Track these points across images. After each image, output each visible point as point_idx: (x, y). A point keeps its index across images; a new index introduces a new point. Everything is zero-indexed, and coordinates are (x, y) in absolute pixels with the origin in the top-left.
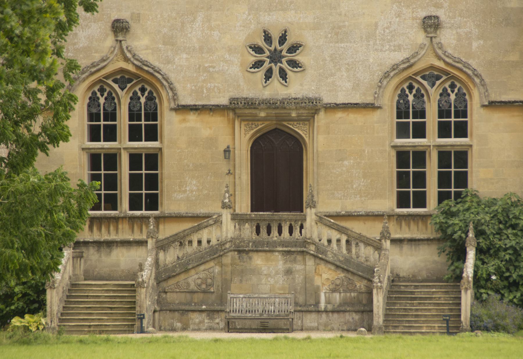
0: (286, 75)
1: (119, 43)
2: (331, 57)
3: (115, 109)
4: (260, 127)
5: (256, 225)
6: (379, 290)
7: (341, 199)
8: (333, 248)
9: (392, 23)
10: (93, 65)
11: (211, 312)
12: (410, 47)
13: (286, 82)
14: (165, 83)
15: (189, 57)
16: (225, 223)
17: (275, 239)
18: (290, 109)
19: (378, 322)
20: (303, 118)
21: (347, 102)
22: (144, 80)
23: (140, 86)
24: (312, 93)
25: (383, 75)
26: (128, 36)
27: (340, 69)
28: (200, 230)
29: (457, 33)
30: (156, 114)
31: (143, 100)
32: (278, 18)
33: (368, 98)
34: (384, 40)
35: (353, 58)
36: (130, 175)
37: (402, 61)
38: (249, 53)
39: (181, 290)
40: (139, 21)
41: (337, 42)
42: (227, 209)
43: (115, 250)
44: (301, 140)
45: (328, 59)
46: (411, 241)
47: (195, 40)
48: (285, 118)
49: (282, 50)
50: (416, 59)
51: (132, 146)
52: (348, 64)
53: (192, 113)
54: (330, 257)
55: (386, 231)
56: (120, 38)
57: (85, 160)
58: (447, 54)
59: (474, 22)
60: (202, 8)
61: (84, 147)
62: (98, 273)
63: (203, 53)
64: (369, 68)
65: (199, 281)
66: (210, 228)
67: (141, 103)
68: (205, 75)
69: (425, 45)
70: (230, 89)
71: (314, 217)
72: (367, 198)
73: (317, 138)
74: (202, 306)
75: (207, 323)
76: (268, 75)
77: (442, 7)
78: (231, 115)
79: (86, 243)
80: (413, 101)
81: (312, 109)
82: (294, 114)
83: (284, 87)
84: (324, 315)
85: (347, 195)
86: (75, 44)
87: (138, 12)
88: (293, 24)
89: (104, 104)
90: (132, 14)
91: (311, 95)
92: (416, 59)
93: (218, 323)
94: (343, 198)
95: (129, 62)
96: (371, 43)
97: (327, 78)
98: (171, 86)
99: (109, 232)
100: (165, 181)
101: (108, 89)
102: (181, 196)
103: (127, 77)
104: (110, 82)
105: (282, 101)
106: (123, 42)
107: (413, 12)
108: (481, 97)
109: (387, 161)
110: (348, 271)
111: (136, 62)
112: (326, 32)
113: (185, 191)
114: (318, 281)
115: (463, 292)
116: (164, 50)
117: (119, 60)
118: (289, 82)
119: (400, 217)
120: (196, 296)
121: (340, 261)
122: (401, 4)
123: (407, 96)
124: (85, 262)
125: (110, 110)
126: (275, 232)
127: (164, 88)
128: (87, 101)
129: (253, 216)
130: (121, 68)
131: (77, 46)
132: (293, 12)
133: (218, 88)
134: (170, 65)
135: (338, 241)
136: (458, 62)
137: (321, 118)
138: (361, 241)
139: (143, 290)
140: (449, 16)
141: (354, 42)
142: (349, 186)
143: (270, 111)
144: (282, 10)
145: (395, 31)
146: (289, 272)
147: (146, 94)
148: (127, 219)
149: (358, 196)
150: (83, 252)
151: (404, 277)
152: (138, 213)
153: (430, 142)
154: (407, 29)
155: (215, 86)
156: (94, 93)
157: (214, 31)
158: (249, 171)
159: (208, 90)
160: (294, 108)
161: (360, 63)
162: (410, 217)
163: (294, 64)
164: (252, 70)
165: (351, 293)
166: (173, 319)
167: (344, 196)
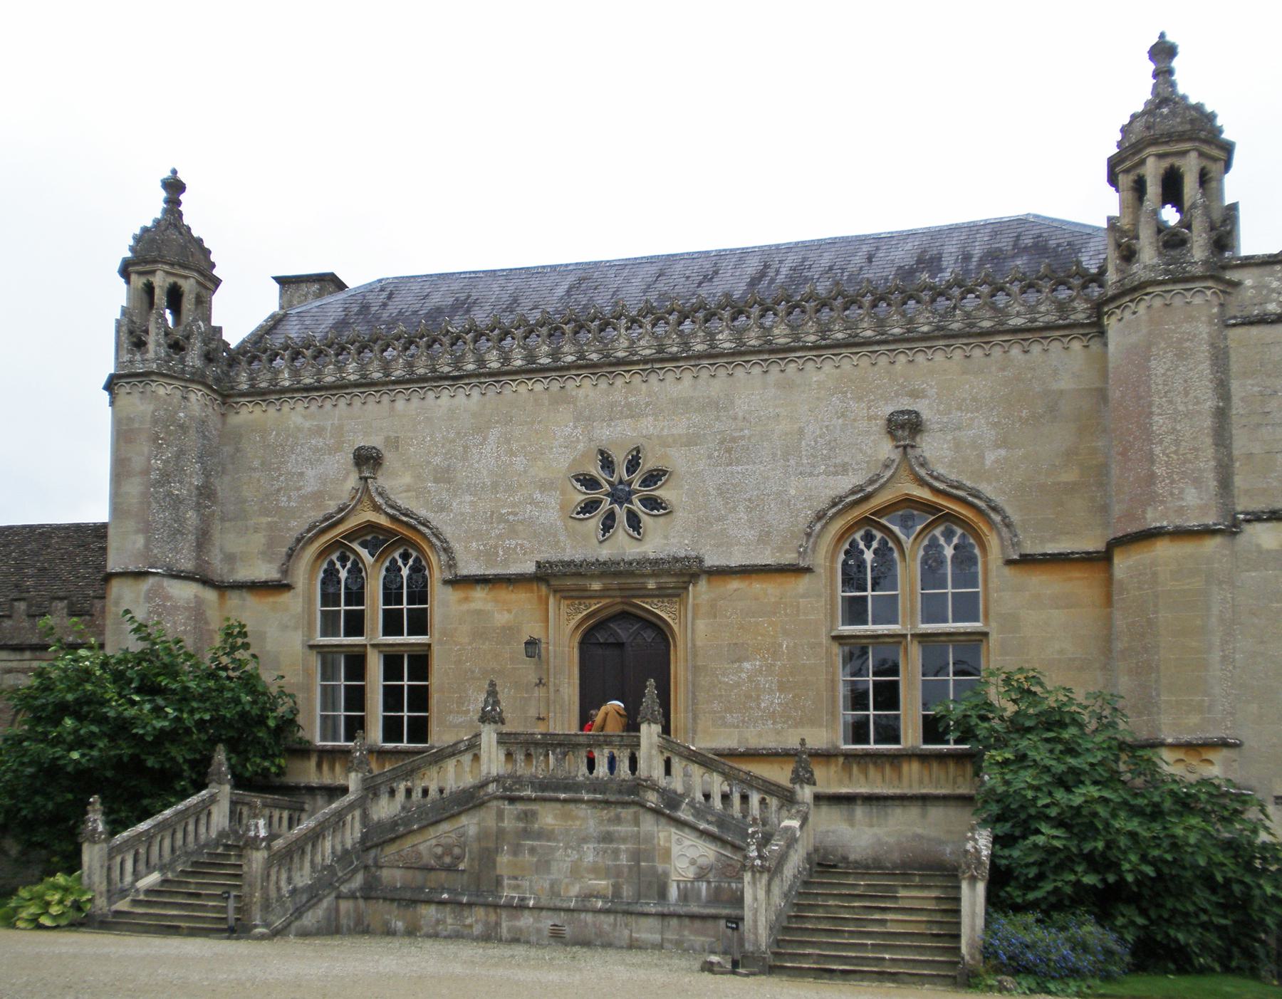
0: (639, 522)
3: (362, 587)
6: (758, 875)
7: (738, 727)
8: (693, 799)
10: (326, 519)
14: (434, 540)
19: (756, 943)
20: (670, 591)
22: (404, 541)
23: (401, 551)
26: (379, 473)
29: (954, 439)
31: (405, 572)
33: (787, 556)
34: (815, 457)
40: (397, 447)
44: (666, 629)
46: (869, 799)
47: (485, 473)
53: (478, 588)
55: (803, 768)
57: (315, 662)
58: (935, 473)
60: (497, 422)
61: (312, 643)
63: (497, 492)
64: (789, 506)
65: (439, 850)
69: (893, 461)
73: (693, 624)
74: (442, 893)
76: (609, 523)
77: (925, 397)
78: (544, 588)
79: (311, 790)
80: (873, 562)
83: (635, 542)
86: (299, 489)
89: (346, 580)
90: (387, 439)
93: (471, 926)
104: (356, 546)
106: (369, 481)
108: (1003, 547)
109: (824, 661)
111: (389, 511)
115: (965, 886)
119: (848, 756)
120: (433, 875)
122: (846, 396)
123: (862, 552)
125: (355, 588)
128: (321, 575)
131: (303, 491)
132: (651, 419)
133: (522, 546)
135: (725, 797)
136: (957, 488)
137: (701, 592)
140: (938, 410)
141: (761, 462)
142: (753, 705)
144: (632, 417)
147: (411, 562)
149: (770, 722)
151: (856, 862)
154: (860, 438)
155: (516, 547)
158: (577, 682)
159: (507, 550)
161: (772, 497)
162: (868, 759)
163: (653, 504)
164: (581, 516)
167: (743, 721)
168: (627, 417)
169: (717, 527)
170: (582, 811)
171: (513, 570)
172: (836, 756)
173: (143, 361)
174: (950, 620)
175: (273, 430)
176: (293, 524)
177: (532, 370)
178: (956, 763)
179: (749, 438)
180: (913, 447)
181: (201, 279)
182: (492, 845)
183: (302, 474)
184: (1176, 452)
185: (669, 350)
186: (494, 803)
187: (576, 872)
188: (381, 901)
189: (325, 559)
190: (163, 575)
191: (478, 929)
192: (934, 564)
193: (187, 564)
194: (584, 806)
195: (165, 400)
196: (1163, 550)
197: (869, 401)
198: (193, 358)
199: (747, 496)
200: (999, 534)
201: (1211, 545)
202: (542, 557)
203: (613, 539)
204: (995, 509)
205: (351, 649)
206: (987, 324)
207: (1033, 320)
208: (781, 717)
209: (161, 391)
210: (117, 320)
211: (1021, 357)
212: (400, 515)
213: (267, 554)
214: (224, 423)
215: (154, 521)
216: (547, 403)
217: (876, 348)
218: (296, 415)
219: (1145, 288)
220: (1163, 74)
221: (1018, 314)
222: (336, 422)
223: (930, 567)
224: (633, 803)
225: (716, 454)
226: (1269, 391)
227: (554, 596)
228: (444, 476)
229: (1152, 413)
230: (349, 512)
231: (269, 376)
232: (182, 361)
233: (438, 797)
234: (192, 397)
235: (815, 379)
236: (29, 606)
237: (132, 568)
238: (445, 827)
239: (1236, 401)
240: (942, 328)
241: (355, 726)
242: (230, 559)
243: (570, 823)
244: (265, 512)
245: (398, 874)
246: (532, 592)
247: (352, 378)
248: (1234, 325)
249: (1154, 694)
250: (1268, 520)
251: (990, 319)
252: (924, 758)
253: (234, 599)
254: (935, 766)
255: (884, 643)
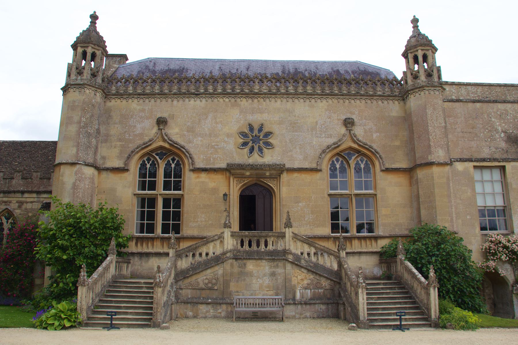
1: (160, 130)
2: (290, 140)
3: (156, 171)
4: (246, 182)
5: (248, 240)
7: (297, 227)
9: (326, 122)
10: (144, 144)
11: (216, 303)
12: (337, 135)
13: (262, 155)
14: (187, 154)
15: (203, 139)
16: (226, 239)
17: (263, 250)
18: (266, 170)
20: (273, 176)
21: (300, 167)
23: (172, 157)
24: (279, 162)
25: (321, 151)
26: (166, 127)
27: (295, 147)
28: (208, 243)
29: (364, 129)
30: (181, 174)
31: (173, 166)
32: (258, 117)
34: (322, 131)
35: (303, 141)
36: (163, 211)
37: (334, 143)
38: (240, 137)
39: (194, 288)
40: (173, 118)
41: (293, 132)
42: (227, 228)
43: (151, 259)
44: (270, 189)
45: (288, 141)
47: (206, 129)
48: (261, 176)
49: (260, 136)
50: (341, 142)
51: (165, 193)
52: (300, 145)
53: (203, 173)
54: (303, 263)
56: (161, 127)
57: (135, 201)
59: (373, 123)
60: (212, 111)
61: (135, 193)
62: (140, 274)
63: (211, 137)
64: (313, 147)
65: (207, 281)
66: (215, 242)
67: (172, 168)
68: (212, 150)
69: (346, 134)
70: (228, 159)
71: (291, 234)
72: (314, 227)
74: (208, 299)
75: (212, 313)
76: (252, 150)
77: (354, 114)
78: (228, 174)
79: (133, 254)
81: (279, 170)
82: (268, 174)
83: (261, 158)
84: (299, 306)
85: (301, 225)
86: (134, 132)
87: (173, 113)
88: (266, 121)
89: (149, 168)
90: (170, 115)
91: (278, 163)
92: (341, 142)
93: (221, 313)
94: (298, 226)
95: (166, 142)
96: (314, 133)
97: (288, 153)
98: (191, 156)
99: (148, 247)
100: (185, 215)
101: (152, 159)
102: (194, 224)
103: (164, 152)
105: (261, 165)
106: (163, 130)
107: (338, 116)
110: (316, 274)
112: (286, 126)
113: (197, 221)
114: (294, 281)
116: (187, 135)
117: (160, 141)
118: (264, 155)
120: (204, 291)
121: (311, 267)
124: (132, 266)
125: (153, 171)
126: (254, 245)
127: (186, 158)
128: (140, 166)
129: (247, 233)
130: (161, 145)
131: (135, 133)
133: (220, 157)
134: (191, 144)
137: (285, 177)
138: (325, 252)
139: (160, 290)
141: (304, 132)
143: (252, 171)
144: (260, 113)
145: (328, 126)
146: (273, 274)
148: (160, 239)
149: (308, 225)
150: (130, 260)
152: (166, 235)
153: (352, 192)
155: (218, 157)
156: (144, 161)
157: (218, 124)
159: (214, 159)
160: (268, 169)
161: (308, 144)
164: (241, 147)
165: (318, 289)
166: (187, 309)
168: (258, 113)
169: (289, 154)
170: (264, 263)
171: (217, 166)
172: (331, 238)
173: (81, 79)
174: (364, 189)
175: (124, 109)
176: (130, 145)
177: (224, 94)
178: (364, 240)
179: (300, 123)
180: (352, 130)
181: (103, 51)
182: (228, 278)
183: (135, 126)
184: (436, 138)
185: (273, 91)
186: (231, 261)
187: (261, 287)
188: (183, 304)
189: (142, 159)
190: (82, 164)
191: (223, 314)
192: (358, 170)
193: (90, 160)
194: (264, 261)
195: (88, 95)
196: (435, 170)
197: (338, 114)
198: (99, 80)
199: (299, 143)
200: (379, 161)
201: (447, 168)
202: (228, 162)
203: (253, 156)
204: (377, 152)
205: (151, 196)
206: (371, 93)
207: (384, 93)
208: (312, 224)
209: (87, 91)
210: (69, 64)
211: (381, 104)
212: (173, 144)
213: (119, 157)
214: (105, 105)
215: (81, 142)
216: (230, 106)
217: (339, 97)
218: (135, 105)
219: (424, 87)
220: (416, 27)
221: (380, 91)
222: (150, 107)
223: (357, 171)
224: (284, 259)
225: (289, 128)
226: (455, 122)
227: (232, 177)
228: (191, 130)
229: (428, 126)
230: (154, 142)
231: (124, 88)
232: (96, 80)
233: (206, 259)
234: (98, 94)
235: (320, 105)
236: (4, 175)
237: (70, 161)
238: (209, 271)
239: (448, 125)
240: (358, 93)
241: (151, 229)
242: (104, 158)
243: (259, 268)
244: (120, 140)
245: (189, 291)
246: (223, 175)
247: (157, 91)
248: (445, 101)
249: (434, 216)
250: (459, 161)
251: (372, 91)
252: (359, 238)
253: (104, 174)
254: (363, 241)
255: (344, 197)
